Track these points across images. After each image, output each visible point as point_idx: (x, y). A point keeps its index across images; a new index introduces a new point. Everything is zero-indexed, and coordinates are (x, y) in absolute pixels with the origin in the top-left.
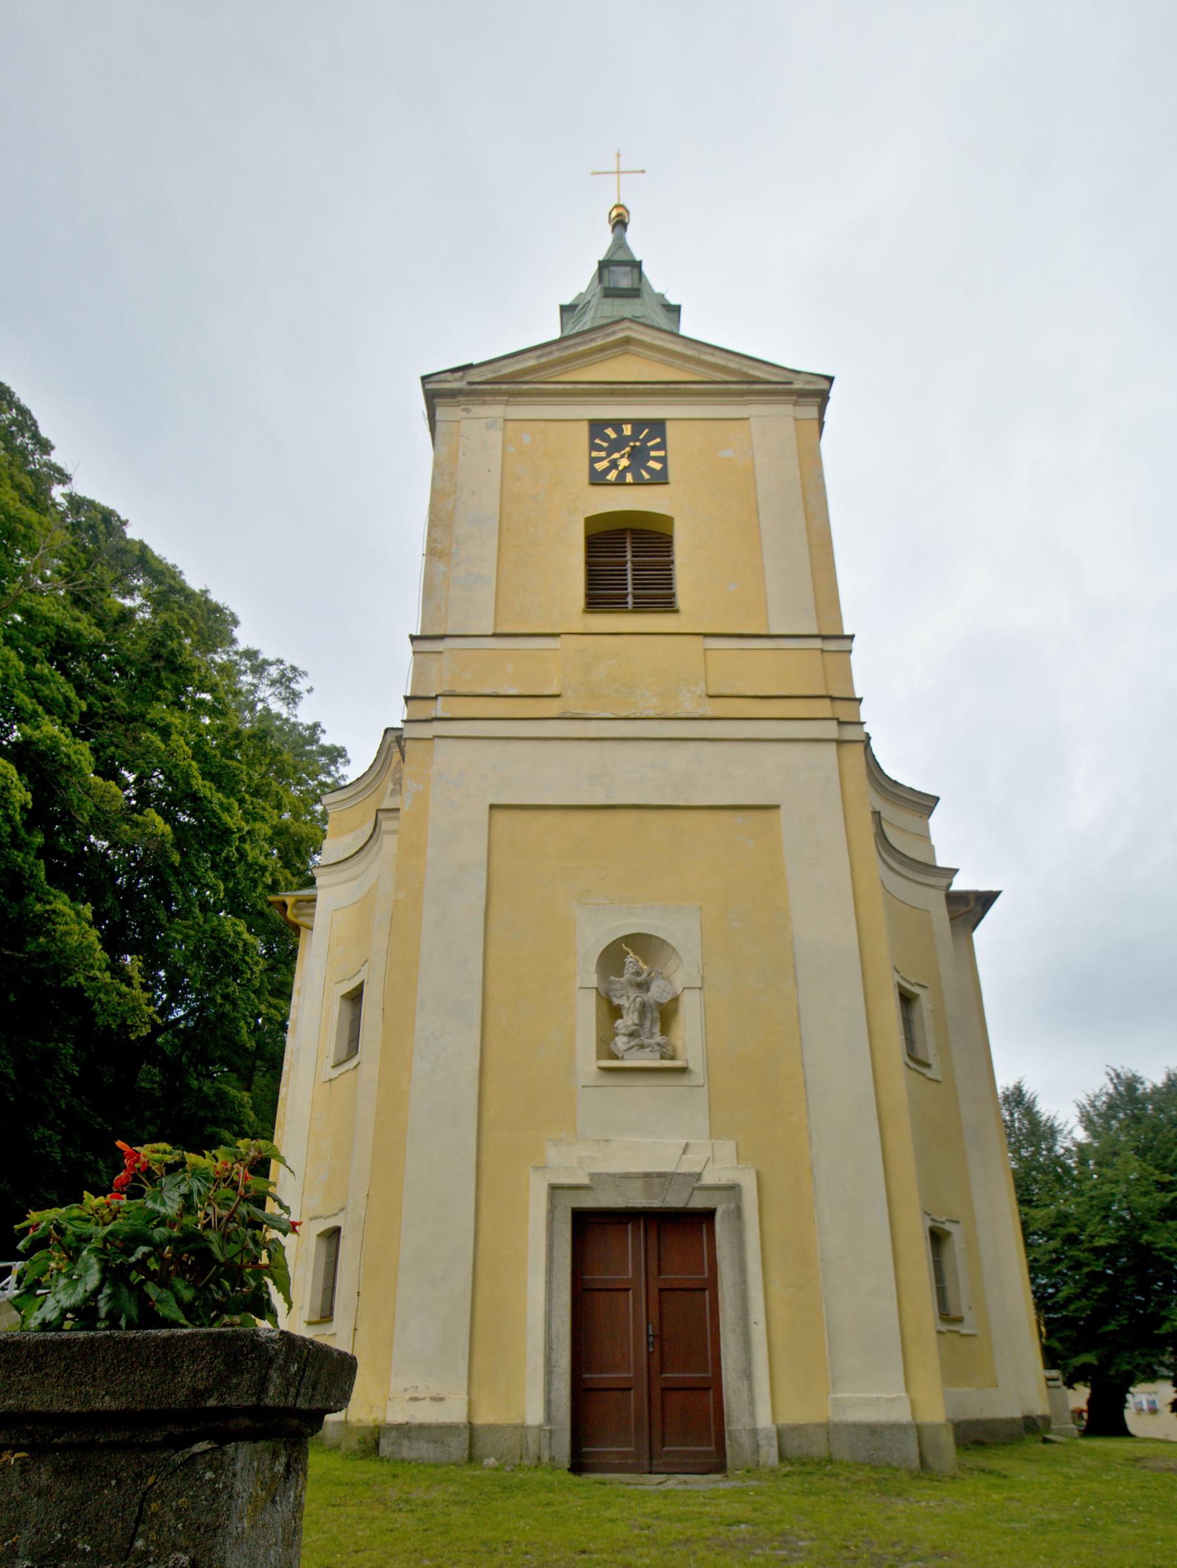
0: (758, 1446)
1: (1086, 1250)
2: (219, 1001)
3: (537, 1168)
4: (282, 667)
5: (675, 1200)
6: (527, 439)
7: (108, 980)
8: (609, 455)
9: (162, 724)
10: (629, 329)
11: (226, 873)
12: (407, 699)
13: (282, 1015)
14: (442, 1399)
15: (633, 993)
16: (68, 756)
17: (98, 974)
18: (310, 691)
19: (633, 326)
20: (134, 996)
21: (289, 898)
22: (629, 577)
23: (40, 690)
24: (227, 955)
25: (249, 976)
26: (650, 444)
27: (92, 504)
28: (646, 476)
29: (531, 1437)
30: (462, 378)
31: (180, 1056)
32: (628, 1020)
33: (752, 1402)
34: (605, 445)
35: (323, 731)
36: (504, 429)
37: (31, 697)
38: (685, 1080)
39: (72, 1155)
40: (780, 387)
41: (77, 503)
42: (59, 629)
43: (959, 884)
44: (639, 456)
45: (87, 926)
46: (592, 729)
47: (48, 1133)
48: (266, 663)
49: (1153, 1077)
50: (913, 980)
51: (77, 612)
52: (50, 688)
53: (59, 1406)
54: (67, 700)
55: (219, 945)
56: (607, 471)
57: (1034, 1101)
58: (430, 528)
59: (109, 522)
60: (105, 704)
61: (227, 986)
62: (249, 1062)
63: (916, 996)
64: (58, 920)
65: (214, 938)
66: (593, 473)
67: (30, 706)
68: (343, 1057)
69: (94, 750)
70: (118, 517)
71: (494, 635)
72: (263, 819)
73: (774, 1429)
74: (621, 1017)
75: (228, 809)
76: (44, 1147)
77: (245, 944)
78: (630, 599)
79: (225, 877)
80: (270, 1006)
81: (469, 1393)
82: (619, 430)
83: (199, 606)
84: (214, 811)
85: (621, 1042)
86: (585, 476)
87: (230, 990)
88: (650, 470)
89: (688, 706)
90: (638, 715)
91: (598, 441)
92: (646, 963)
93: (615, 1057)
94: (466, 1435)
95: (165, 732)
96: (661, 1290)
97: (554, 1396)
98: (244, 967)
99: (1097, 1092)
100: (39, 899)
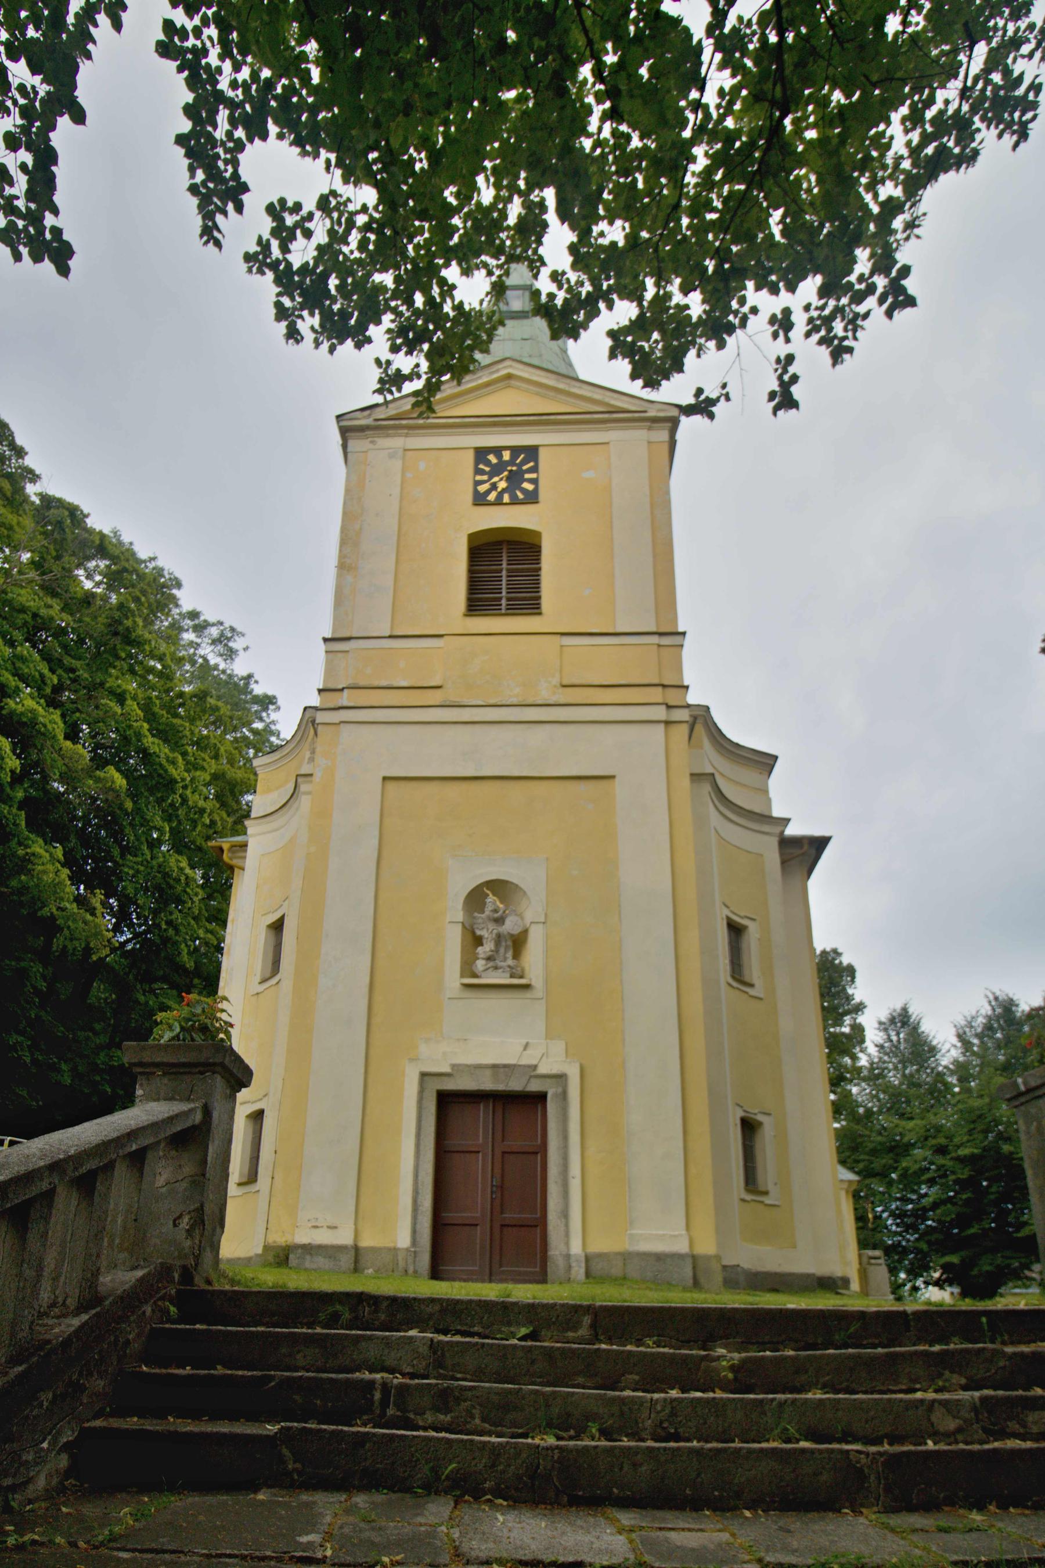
0: (570, 1267)
1: (952, 1159)
2: (164, 926)
3: (411, 1060)
4: (222, 628)
5: (515, 1085)
6: (422, 466)
7: (76, 910)
8: (490, 479)
9: (119, 691)
10: (511, 366)
11: (170, 815)
12: (320, 691)
13: (217, 939)
14: (336, 1227)
15: (491, 926)
16: (45, 726)
17: (68, 905)
18: (246, 649)
19: (514, 364)
20: (103, 928)
21: (225, 843)
22: (504, 583)
23: (21, 669)
24: (171, 887)
25: (190, 905)
26: (525, 468)
27: (60, 501)
28: (520, 496)
29: (401, 1257)
30: (369, 416)
31: (127, 974)
32: (488, 947)
33: (567, 1234)
34: (487, 469)
35: (256, 682)
36: (404, 458)
37: (14, 675)
38: (528, 994)
39: (40, 1058)
40: (636, 415)
41: (48, 501)
42: (35, 615)
43: (790, 831)
44: (516, 479)
45: (59, 865)
46: (466, 715)
47: (20, 1039)
48: (206, 625)
49: (1027, 1001)
50: (742, 914)
51: (49, 600)
52: (28, 667)
53: (172, 1061)
54: (42, 676)
55: (164, 878)
56: (488, 492)
57: (919, 1023)
58: (341, 546)
59: (75, 514)
60: (71, 675)
61: (171, 913)
62: (188, 981)
63: (745, 927)
64: (36, 861)
65: (159, 872)
66: (476, 493)
67: (13, 683)
68: (268, 975)
69: (63, 716)
70: (82, 511)
71: (390, 637)
72: (203, 769)
73: (583, 1255)
74: (482, 945)
75: (173, 762)
76: (16, 1051)
77: (187, 878)
78: (504, 602)
79: (169, 819)
80: (207, 931)
81: (356, 1224)
82: (499, 456)
83: (149, 584)
84: (161, 765)
85: (480, 964)
86: (469, 497)
87: (174, 917)
88: (524, 491)
89: (545, 694)
90: (504, 703)
91: (481, 466)
92: (501, 903)
93: (475, 976)
94: (353, 1253)
95: (120, 698)
96: (504, 1153)
97: (418, 1226)
98: (185, 898)
99: (974, 1013)
100: (20, 844)
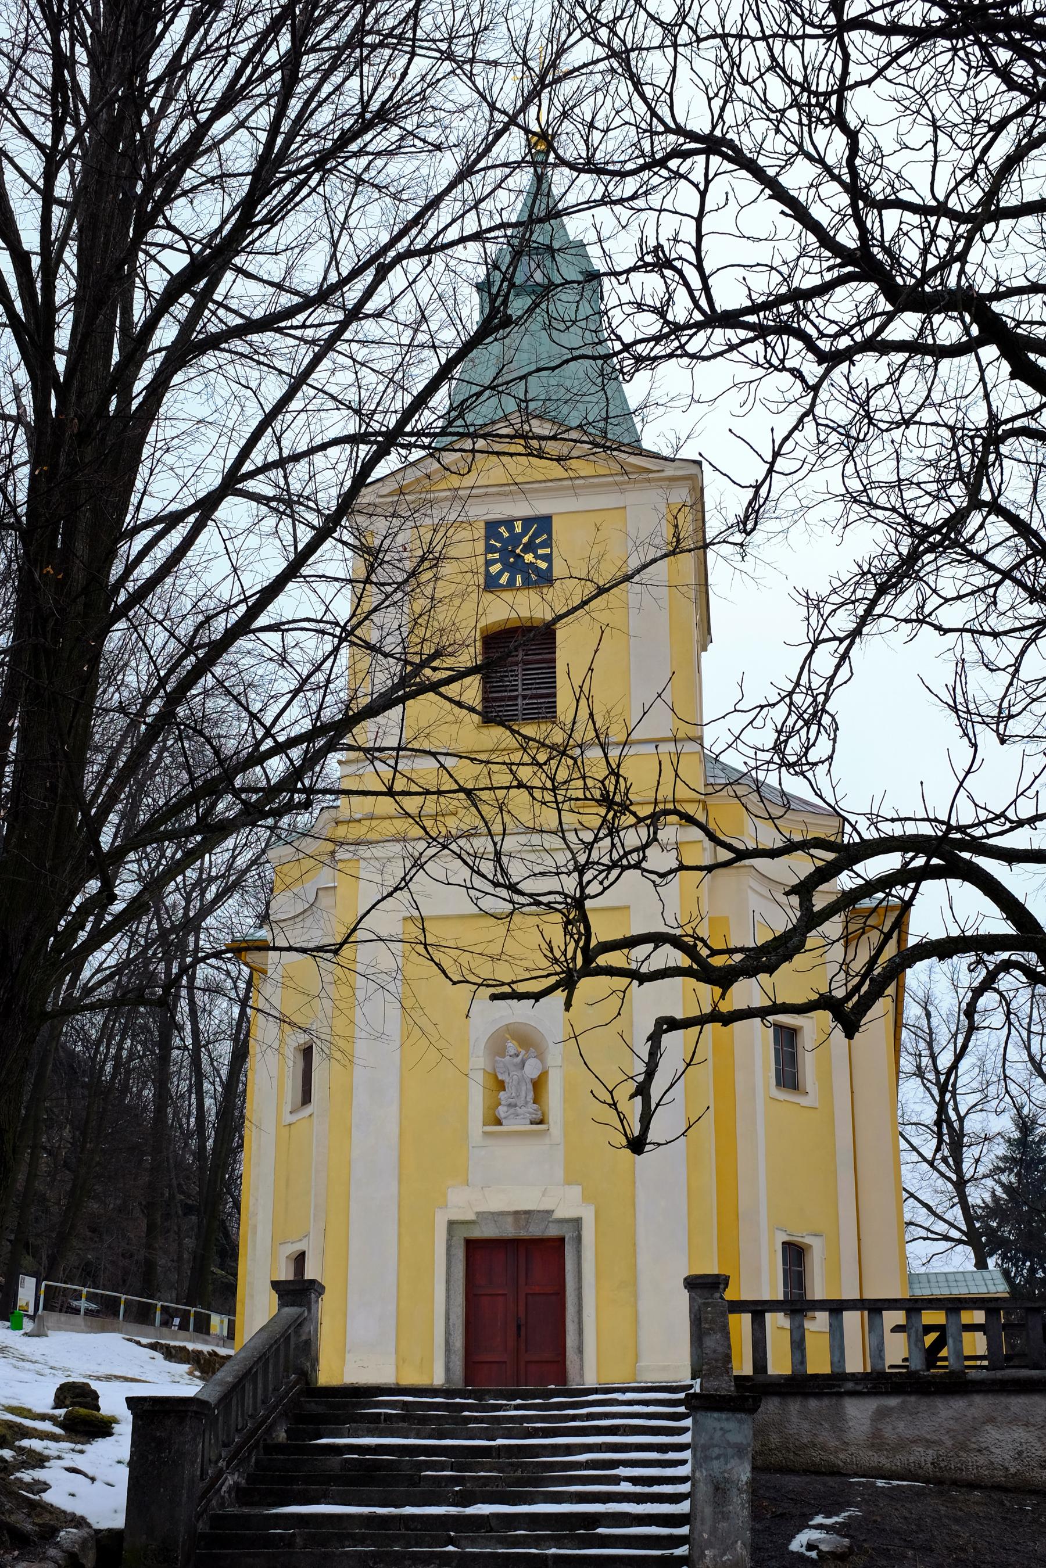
5: (535, 1231)
93: (499, 1123)
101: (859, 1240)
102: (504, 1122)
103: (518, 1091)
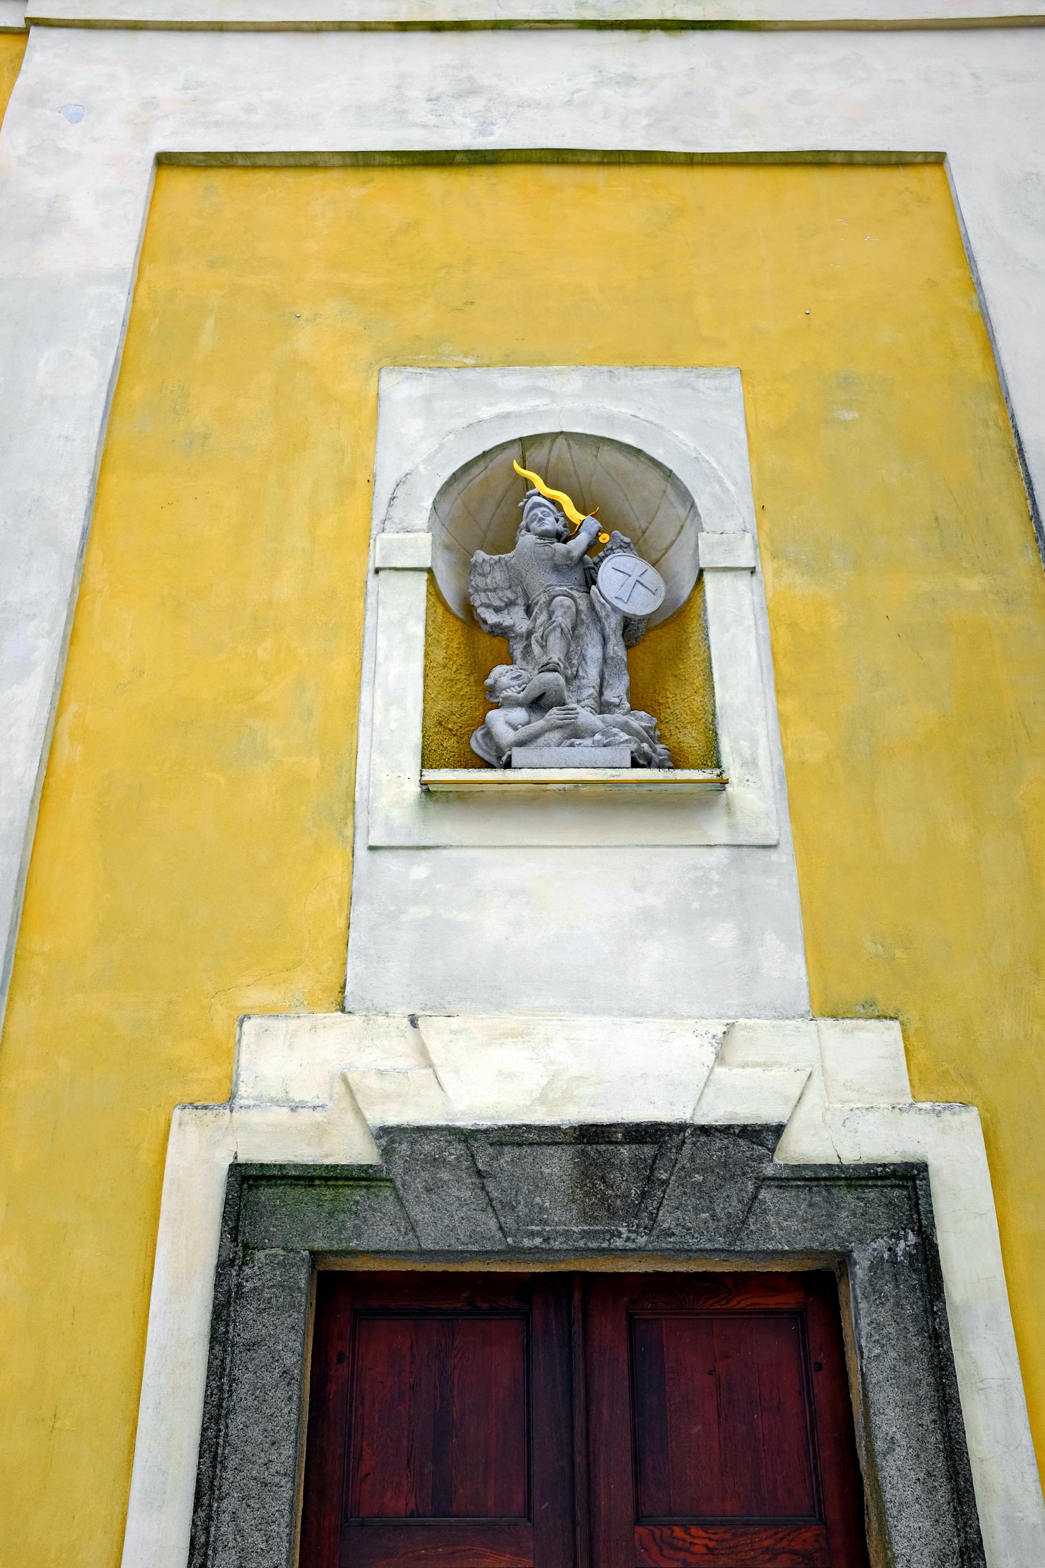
5: (683, 1233)
101: (318, 28)
102: (518, 755)
103: (573, 655)
